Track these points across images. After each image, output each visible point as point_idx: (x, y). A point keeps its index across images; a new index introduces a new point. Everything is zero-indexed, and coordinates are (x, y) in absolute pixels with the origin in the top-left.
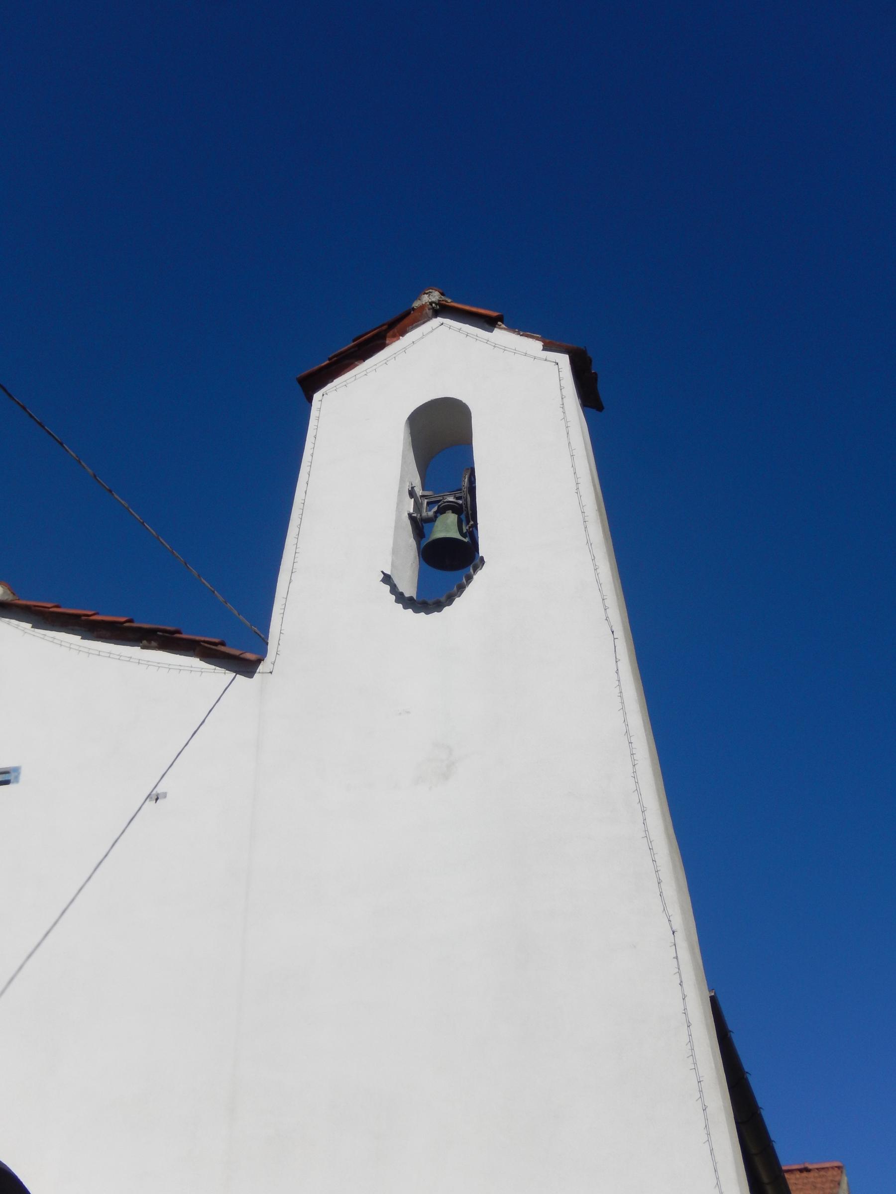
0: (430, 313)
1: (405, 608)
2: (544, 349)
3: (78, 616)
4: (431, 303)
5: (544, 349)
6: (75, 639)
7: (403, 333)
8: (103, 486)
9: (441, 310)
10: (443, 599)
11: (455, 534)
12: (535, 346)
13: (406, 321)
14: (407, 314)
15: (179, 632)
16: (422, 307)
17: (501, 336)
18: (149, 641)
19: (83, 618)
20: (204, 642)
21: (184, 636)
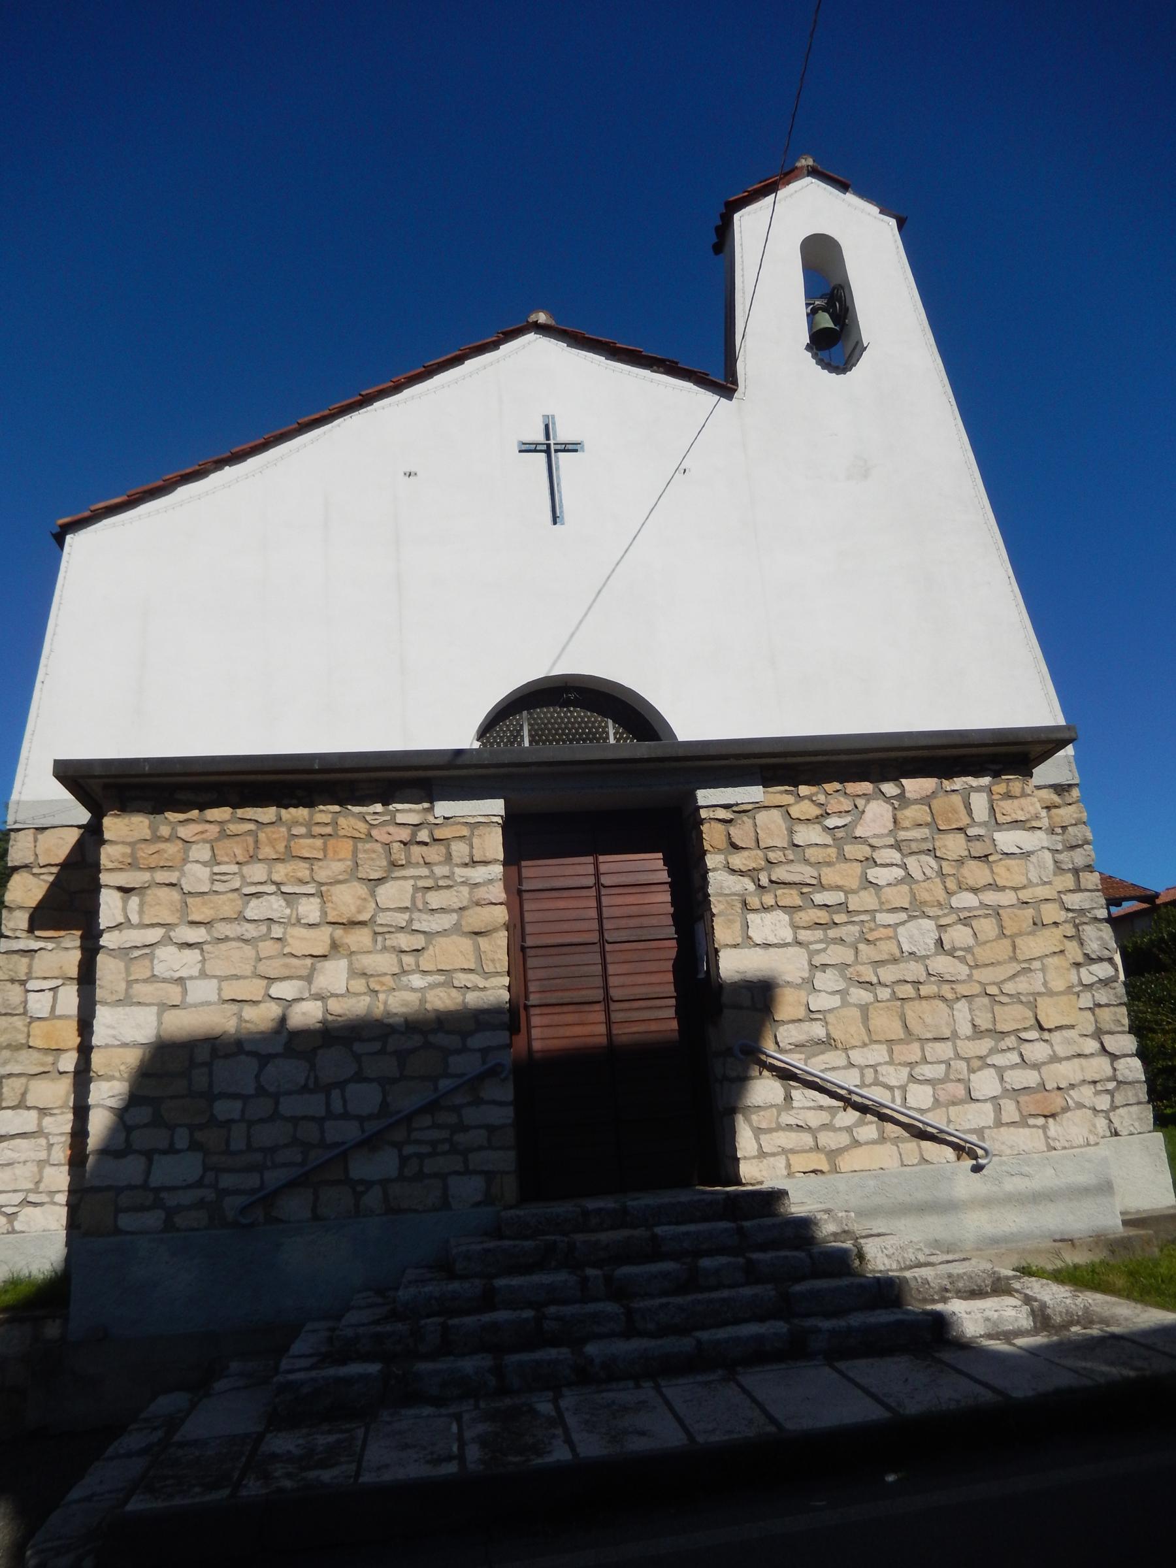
0: (806, 172)
1: (823, 368)
2: (880, 213)
3: (607, 343)
4: (808, 166)
5: (880, 213)
6: (600, 359)
7: (788, 183)
8: (765, 181)
9: (814, 172)
10: (842, 366)
11: (831, 325)
12: (875, 210)
13: (792, 175)
14: (792, 171)
15: (707, 375)
16: (802, 167)
17: (850, 198)
18: (659, 367)
19: (699, 374)
20: (700, 372)
21: (710, 377)
